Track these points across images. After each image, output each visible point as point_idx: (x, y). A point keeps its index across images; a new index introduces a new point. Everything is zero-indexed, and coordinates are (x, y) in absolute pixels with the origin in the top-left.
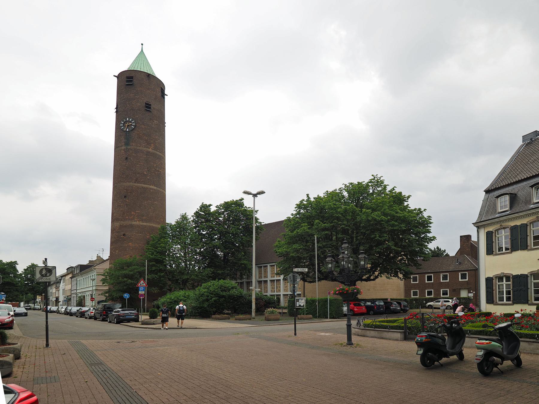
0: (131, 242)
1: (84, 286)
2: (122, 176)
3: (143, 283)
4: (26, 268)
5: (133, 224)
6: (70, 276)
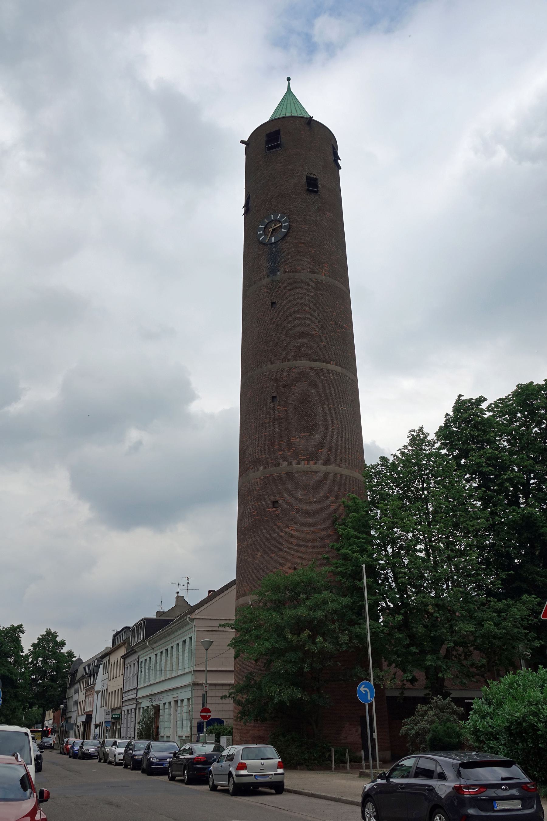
1: (158, 676)
4: (36, 641)
6: (123, 651)
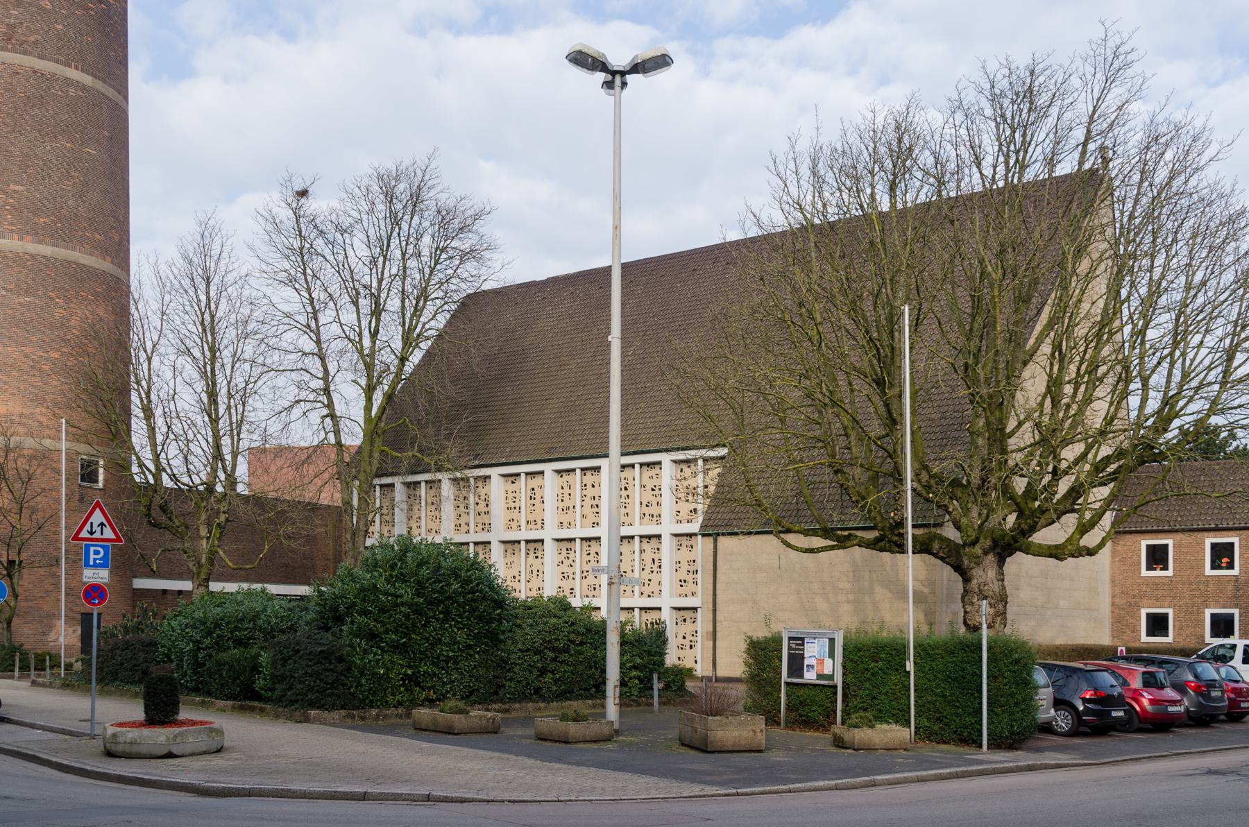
3: (102, 524)
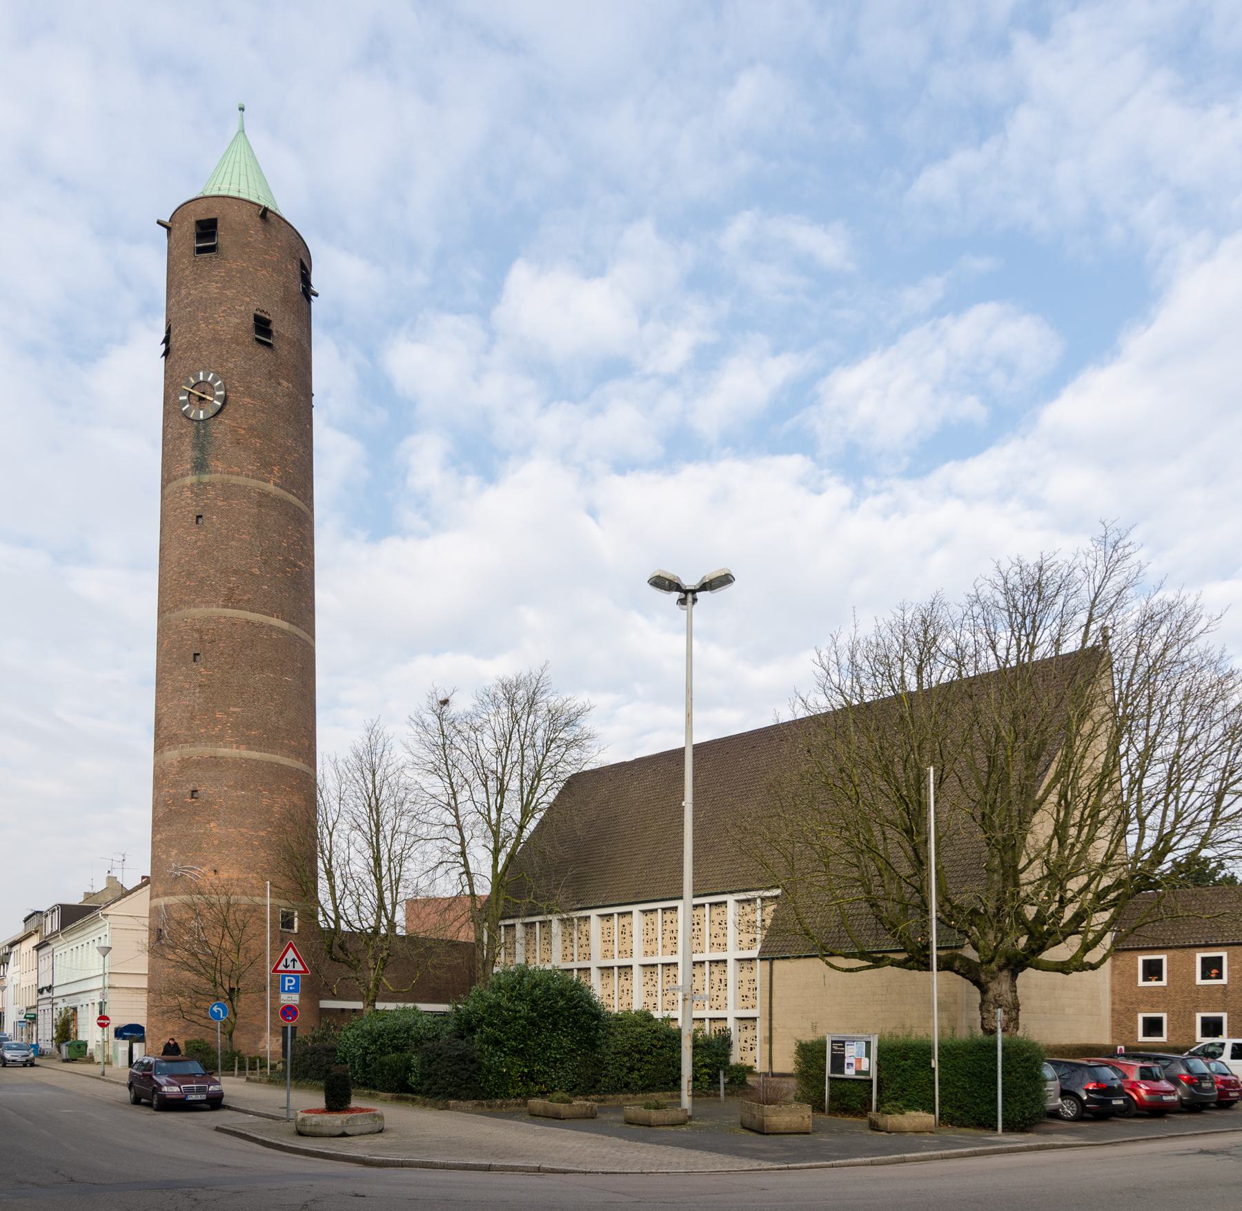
0: (213, 818)
2: (185, 583)
5: (219, 755)
6: (35, 940)
